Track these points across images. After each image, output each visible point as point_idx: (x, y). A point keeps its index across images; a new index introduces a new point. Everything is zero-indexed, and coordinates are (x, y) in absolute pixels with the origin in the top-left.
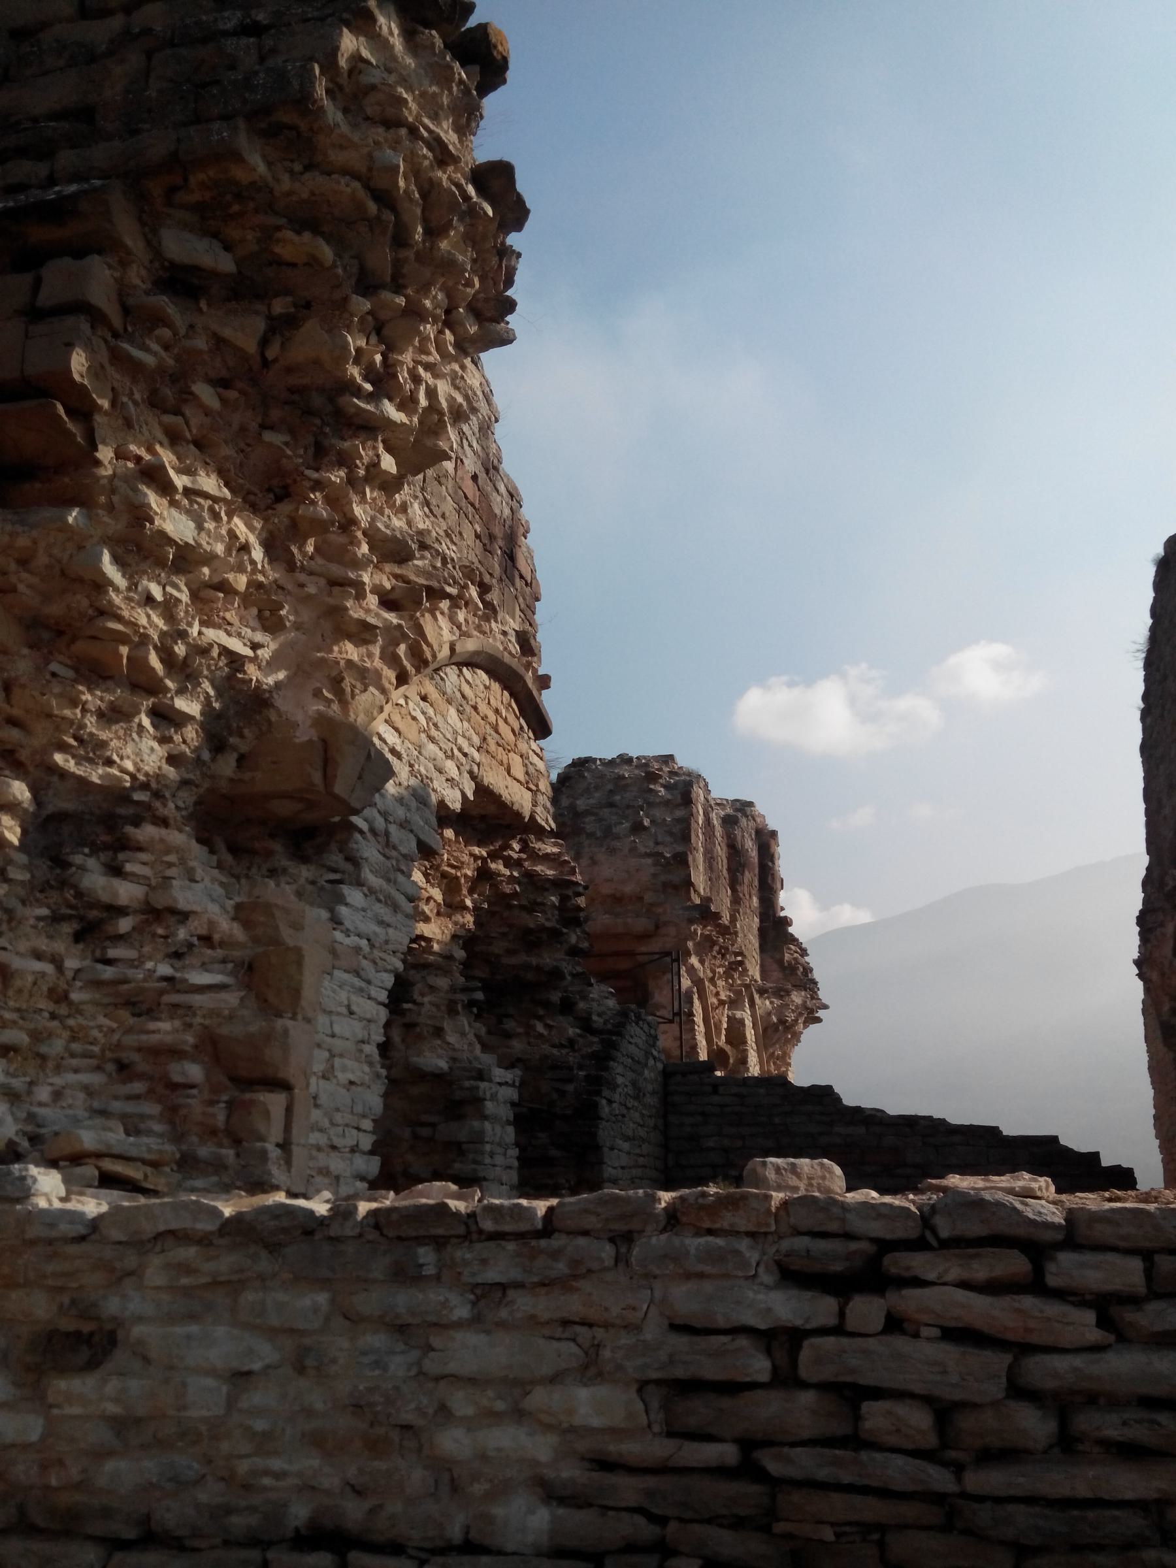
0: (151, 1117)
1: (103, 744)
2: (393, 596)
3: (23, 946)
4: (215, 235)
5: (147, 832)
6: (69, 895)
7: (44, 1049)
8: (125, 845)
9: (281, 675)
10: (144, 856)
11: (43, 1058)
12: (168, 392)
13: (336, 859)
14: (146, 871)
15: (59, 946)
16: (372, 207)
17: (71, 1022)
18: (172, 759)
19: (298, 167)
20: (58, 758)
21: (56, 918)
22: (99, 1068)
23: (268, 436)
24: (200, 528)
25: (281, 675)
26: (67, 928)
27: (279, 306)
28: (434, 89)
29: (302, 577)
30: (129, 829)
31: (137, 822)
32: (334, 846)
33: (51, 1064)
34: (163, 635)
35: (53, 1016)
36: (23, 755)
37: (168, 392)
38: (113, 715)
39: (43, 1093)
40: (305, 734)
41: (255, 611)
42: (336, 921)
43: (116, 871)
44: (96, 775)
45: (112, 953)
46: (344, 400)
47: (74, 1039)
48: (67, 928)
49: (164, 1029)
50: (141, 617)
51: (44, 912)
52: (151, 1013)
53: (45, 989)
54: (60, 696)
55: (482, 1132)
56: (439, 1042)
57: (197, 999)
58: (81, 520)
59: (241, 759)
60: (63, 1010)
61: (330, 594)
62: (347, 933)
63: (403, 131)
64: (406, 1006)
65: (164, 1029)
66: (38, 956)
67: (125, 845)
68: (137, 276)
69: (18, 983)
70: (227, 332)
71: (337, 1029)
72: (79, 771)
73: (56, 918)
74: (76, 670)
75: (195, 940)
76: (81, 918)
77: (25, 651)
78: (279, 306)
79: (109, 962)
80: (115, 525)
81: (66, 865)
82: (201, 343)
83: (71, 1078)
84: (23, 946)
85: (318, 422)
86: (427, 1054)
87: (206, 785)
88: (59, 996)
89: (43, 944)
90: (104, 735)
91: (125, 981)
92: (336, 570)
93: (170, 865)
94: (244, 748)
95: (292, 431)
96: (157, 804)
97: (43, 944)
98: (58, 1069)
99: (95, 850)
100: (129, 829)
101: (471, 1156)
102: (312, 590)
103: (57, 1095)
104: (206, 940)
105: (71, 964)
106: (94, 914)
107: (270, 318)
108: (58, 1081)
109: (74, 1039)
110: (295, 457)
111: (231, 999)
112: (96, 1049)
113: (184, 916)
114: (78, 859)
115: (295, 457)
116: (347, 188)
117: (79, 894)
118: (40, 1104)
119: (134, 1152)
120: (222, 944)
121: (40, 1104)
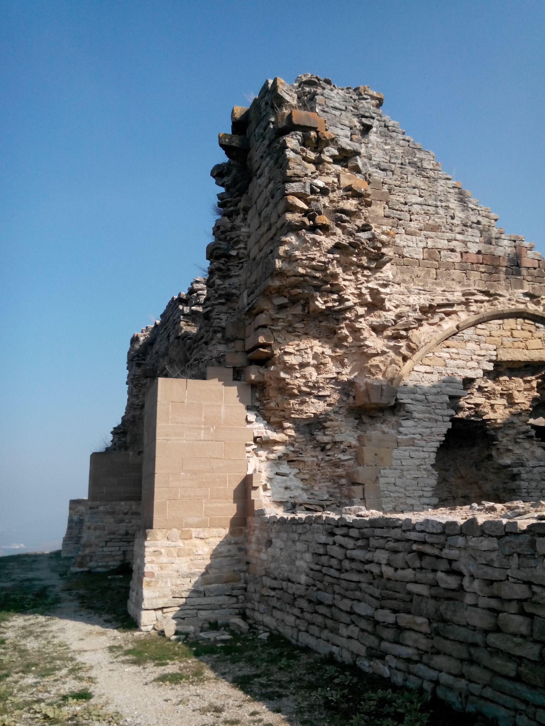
0: (337, 493)
1: (302, 410)
2: (394, 336)
3: (309, 455)
4: (283, 296)
5: (328, 424)
6: (315, 442)
7: (315, 478)
8: (325, 428)
9: (356, 374)
10: (329, 429)
11: (316, 480)
12: (290, 329)
13: (403, 413)
14: (331, 433)
15: (317, 453)
16: (302, 279)
17: (322, 471)
18: (329, 405)
19: (285, 278)
20: (293, 416)
21: (315, 447)
22: (330, 481)
23: (322, 324)
24: (303, 358)
25: (356, 374)
26: (318, 449)
27: (302, 302)
28: (305, 245)
29: (350, 349)
30: (325, 424)
31: (326, 422)
32: (402, 410)
33: (318, 481)
34: (304, 383)
35: (319, 470)
36: (286, 416)
37: (290, 329)
38: (303, 403)
39: (316, 488)
40: (363, 388)
41: (339, 362)
42: (400, 433)
43: (325, 435)
44: (304, 416)
45: (328, 454)
46: (332, 309)
47: (322, 475)
48: (318, 449)
49: (340, 471)
50: (296, 382)
51: (312, 446)
52: (338, 467)
53: (315, 464)
54: (286, 404)
55: (519, 485)
56: (511, 454)
57: (345, 463)
58: (275, 368)
59: (354, 397)
60: (320, 468)
61: (360, 350)
62: (406, 435)
63: (299, 261)
64: (494, 443)
65: (340, 471)
66: (313, 456)
67: (325, 428)
68: (271, 312)
69: (307, 464)
70: (294, 313)
71: (403, 463)
72: (300, 417)
73: (315, 447)
74: (290, 396)
75: (347, 448)
76: (321, 446)
77: (279, 395)
78: (302, 302)
79: (329, 456)
80: (281, 366)
81: (313, 435)
82: (290, 318)
83: (323, 484)
84: (309, 455)
85: (331, 316)
86: (505, 458)
87: (347, 407)
88: (318, 465)
89: (313, 454)
90: (301, 408)
91: (331, 460)
92: (358, 344)
93: (336, 430)
94: (353, 395)
95: (327, 320)
96: (328, 417)
97: (313, 454)
98: (320, 482)
99: (320, 430)
100: (325, 424)
101: (518, 494)
102: (353, 351)
103: (320, 488)
104: (350, 447)
105: (320, 457)
106: (322, 445)
107: (302, 305)
108: (320, 485)
109: (322, 475)
110: (331, 325)
111: (351, 462)
112: (328, 477)
113: (341, 442)
114: (315, 433)
115: (331, 325)
116: (293, 279)
117: (317, 441)
118: (316, 491)
119: (312, 503)
120: (354, 447)
121: (316, 491)
